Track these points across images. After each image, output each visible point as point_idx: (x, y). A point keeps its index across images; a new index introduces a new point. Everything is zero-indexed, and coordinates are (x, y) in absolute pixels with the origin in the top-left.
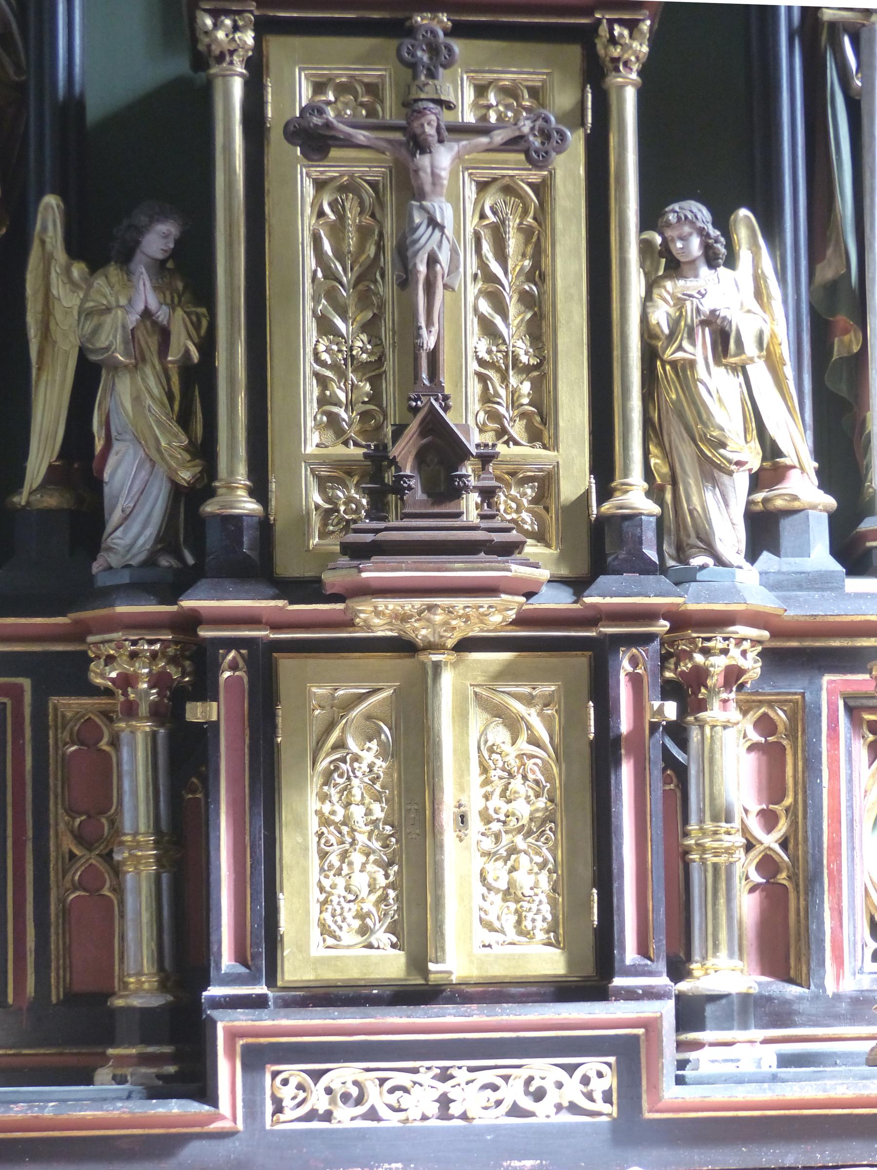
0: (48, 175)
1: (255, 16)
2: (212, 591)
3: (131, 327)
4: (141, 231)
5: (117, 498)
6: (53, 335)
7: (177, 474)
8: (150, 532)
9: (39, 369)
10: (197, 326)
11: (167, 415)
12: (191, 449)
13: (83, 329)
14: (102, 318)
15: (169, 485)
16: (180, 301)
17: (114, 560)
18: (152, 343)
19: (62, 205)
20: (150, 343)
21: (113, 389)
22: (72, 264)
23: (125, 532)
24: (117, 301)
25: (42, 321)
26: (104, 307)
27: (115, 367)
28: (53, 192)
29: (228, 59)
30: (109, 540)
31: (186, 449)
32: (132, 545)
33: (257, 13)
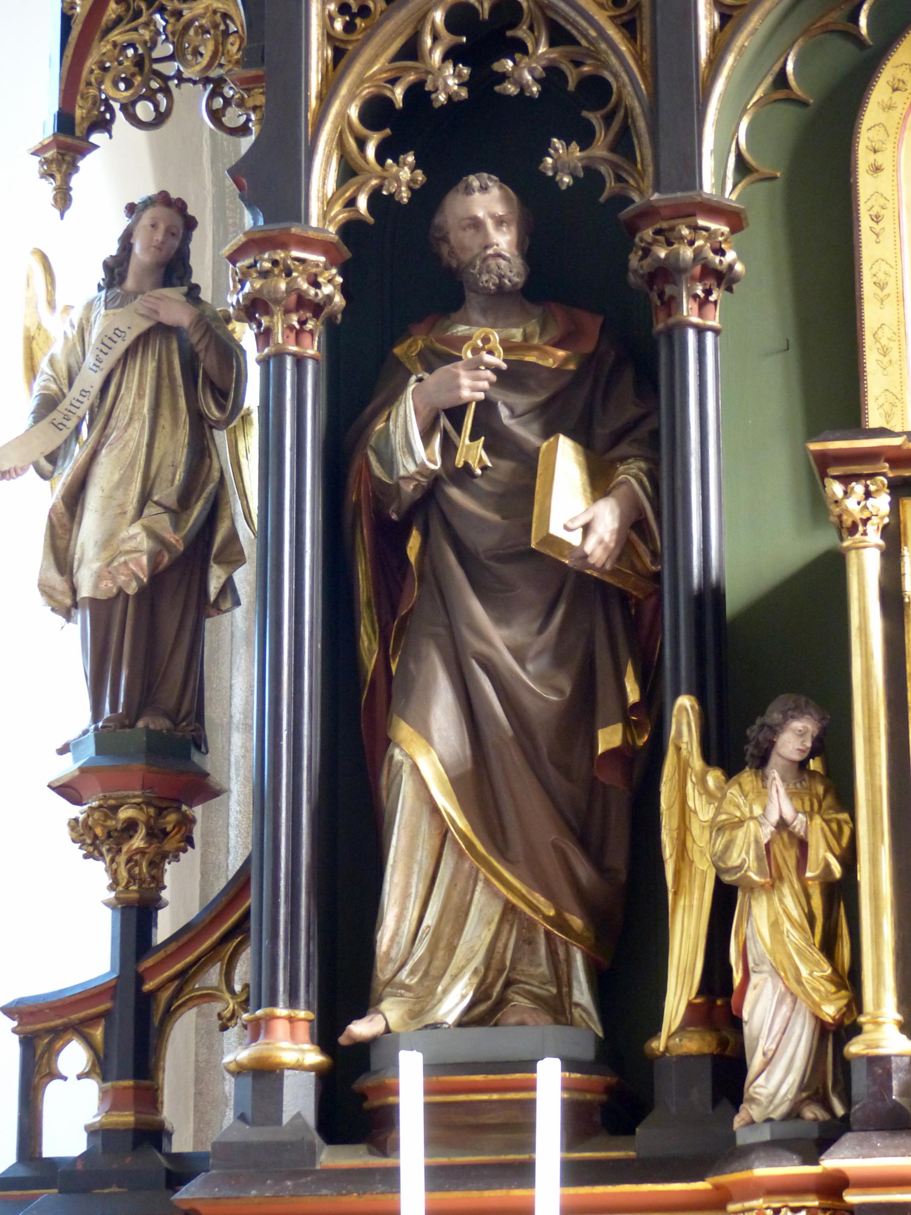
0: (683, 673)
1: (888, 478)
2: (858, 1148)
3: (765, 841)
4: (775, 730)
5: (757, 1039)
6: (690, 853)
7: (821, 1009)
8: (794, 1078)
9: (675, 893)
10: (838, 836)
11: (806, 940)
12: (835, 979)
13: (714, 844)
14: (734, 833)
15: (813, 1022)
16: (820, 806)
17: (756, 1112)
18: (791, 857)
19: (697, 707)
20: (787, 858)
21: (749, 914)
22: (707, 772)
23: (768, 1079)
24: (751, 811)
25: (677, 838)
26: (737, 819)
27: (752, 888)
28: (689, 692)
29: (861, 529)
30: (751, 1089)
31: (831, 981)
32: (775, 1095)
33: (891, 475)
